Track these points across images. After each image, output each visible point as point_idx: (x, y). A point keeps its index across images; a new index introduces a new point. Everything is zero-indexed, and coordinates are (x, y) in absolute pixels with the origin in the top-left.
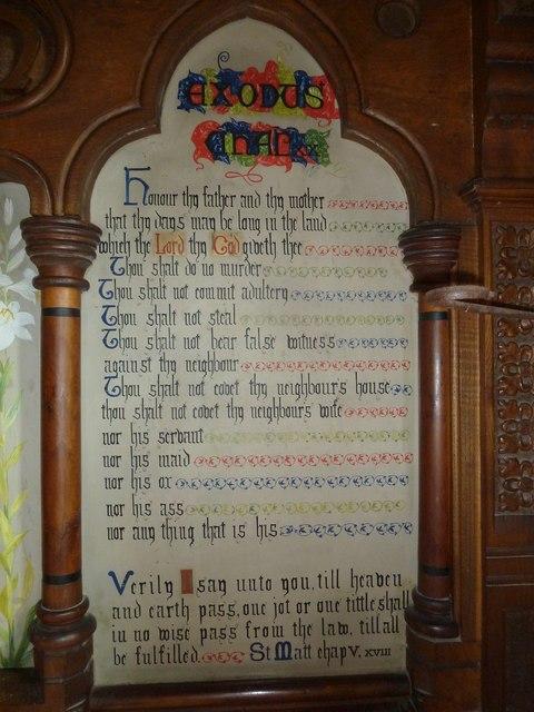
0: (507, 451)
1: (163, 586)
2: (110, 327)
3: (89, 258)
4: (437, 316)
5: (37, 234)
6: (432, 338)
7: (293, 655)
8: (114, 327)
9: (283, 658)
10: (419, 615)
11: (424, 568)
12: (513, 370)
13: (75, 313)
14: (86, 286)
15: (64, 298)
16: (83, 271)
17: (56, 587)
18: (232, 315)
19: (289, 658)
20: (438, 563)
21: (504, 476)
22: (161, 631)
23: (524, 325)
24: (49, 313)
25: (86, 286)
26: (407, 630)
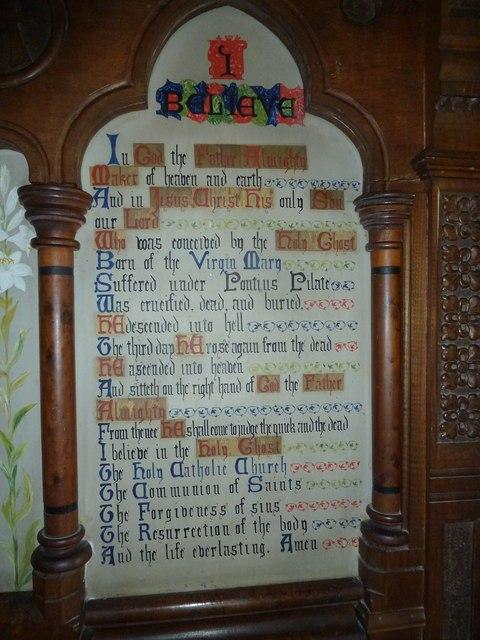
0: (448, 387)
1: (156, 472)
2: (107, 524)
3: (80, 222)
4: (387, 270)
5: (33, 199)
6: (383, 318)
7: (260, 265)
8: (110, 524)
9: (252, 268)
10: (373, 529)
11: (378, 488)
12: (454, 268)
13: (68, 271)
14: (77, 246)
15: (56, 258)
16: (74, 233)
17: (61, 516)
18: (211, 468)
19: (257, 268)
20: (389, 483)
21: (445, 409)
22: (139, 241)
23: (463, 378)
24: (44, 272)
25: (77, 246)
26: (360, 562)
